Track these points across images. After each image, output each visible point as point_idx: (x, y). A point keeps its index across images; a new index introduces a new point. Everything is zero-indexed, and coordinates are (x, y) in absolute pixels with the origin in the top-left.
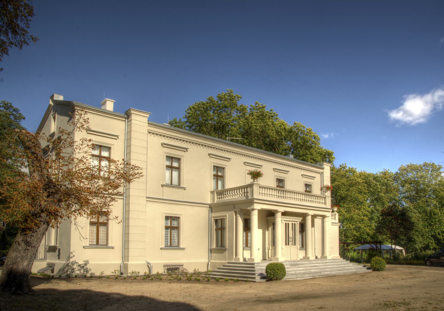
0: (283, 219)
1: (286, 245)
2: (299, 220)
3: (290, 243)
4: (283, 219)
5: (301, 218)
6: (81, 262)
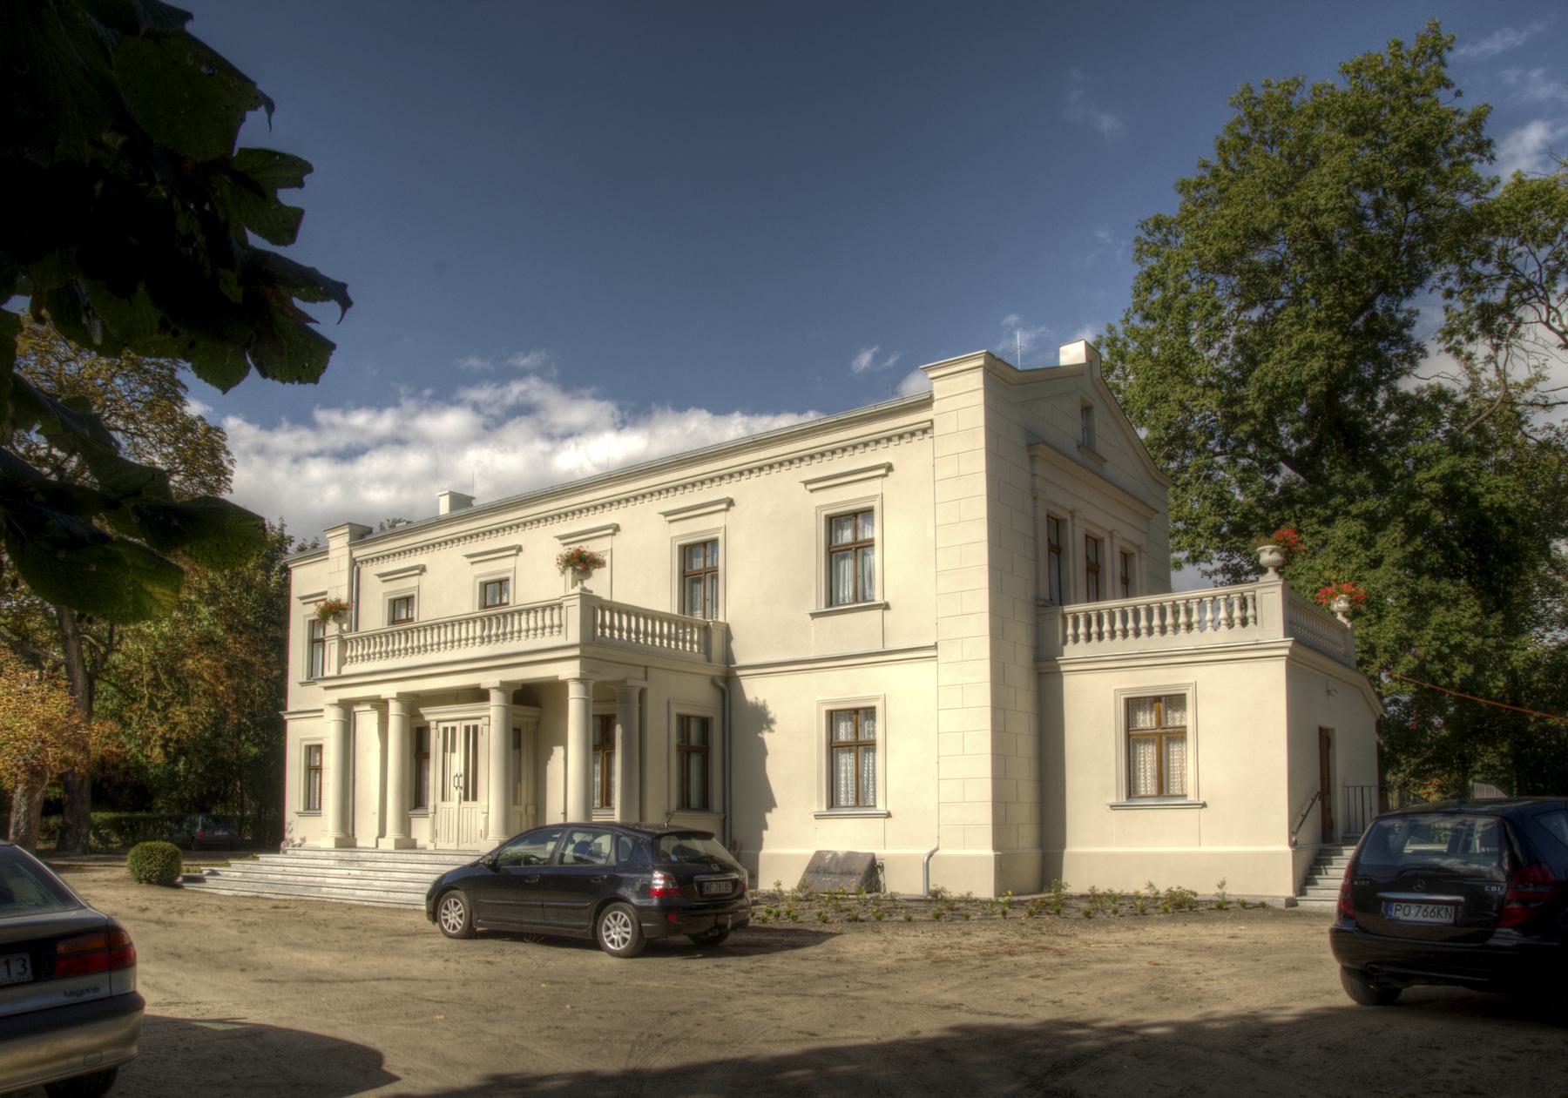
0: (355, 554)
4: (359, 553)
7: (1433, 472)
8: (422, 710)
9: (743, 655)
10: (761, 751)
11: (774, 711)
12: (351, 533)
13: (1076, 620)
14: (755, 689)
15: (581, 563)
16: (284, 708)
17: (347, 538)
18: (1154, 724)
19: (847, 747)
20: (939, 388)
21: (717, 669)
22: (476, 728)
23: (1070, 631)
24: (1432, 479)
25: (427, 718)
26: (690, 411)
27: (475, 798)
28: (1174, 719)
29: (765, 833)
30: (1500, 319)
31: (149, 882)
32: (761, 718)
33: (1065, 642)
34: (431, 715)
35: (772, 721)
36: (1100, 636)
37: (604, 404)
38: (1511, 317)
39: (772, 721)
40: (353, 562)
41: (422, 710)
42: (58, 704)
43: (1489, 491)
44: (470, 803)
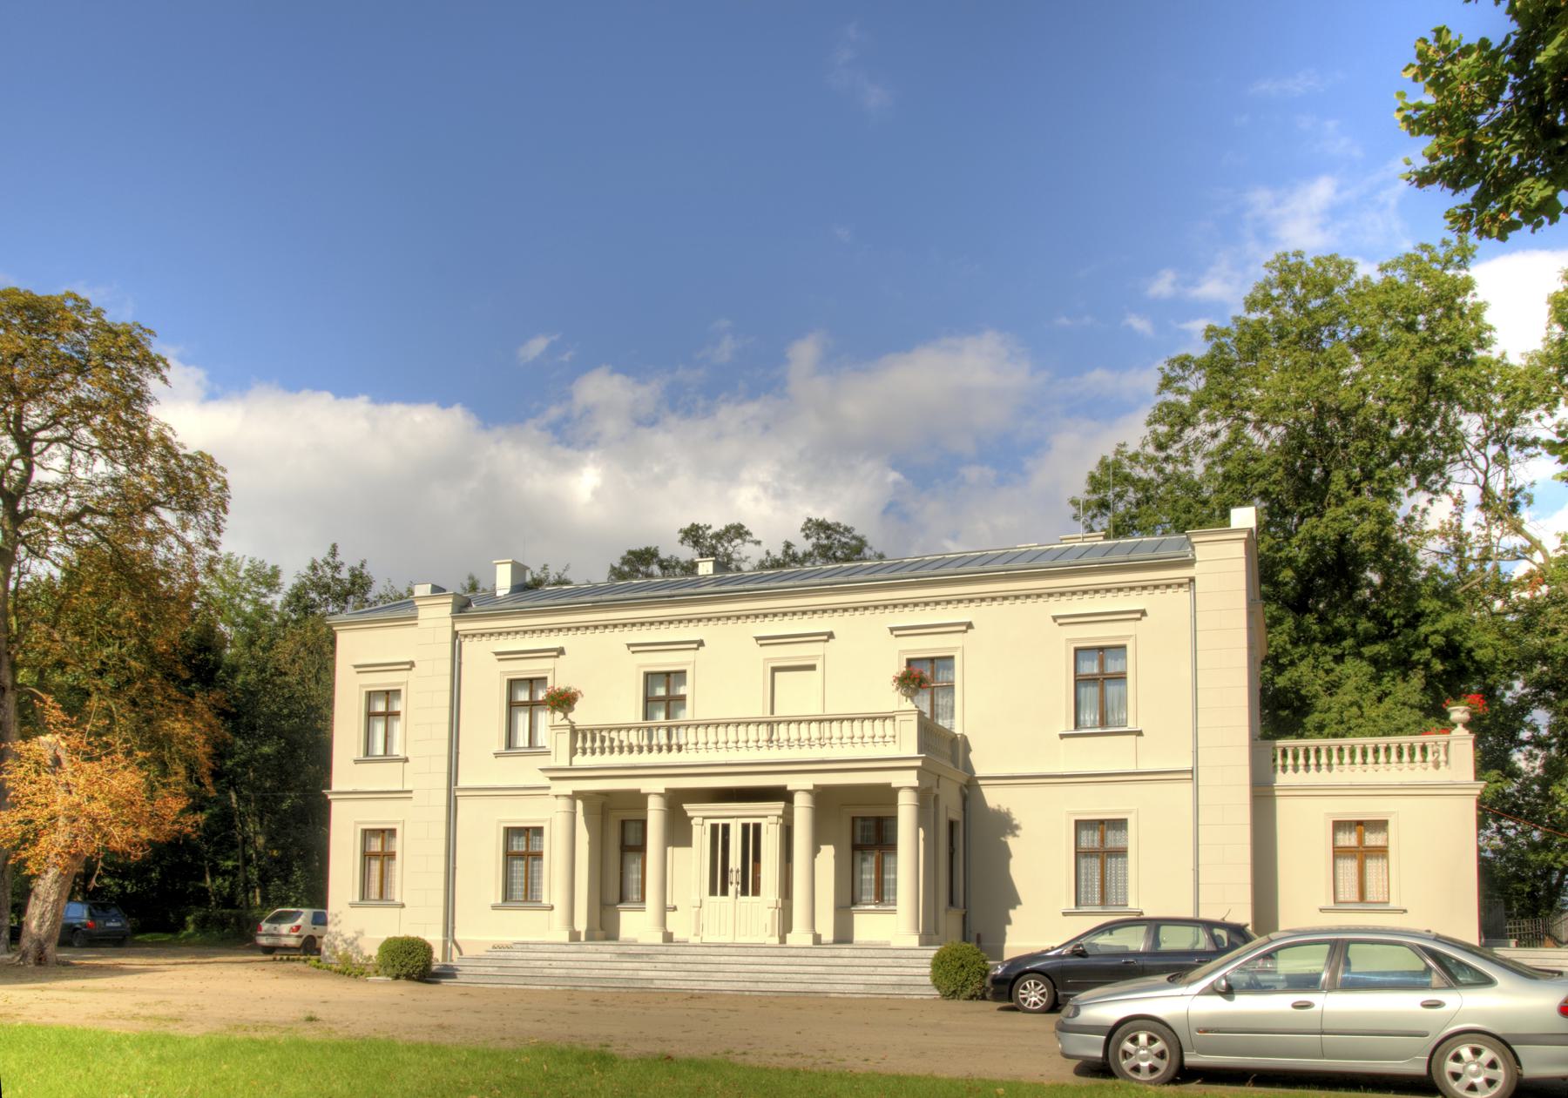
0: (457, 627)
1: (713, 892)
2: (778, 807)
3: (732, 889)
4: (461, 626)
5: (781, 804)
6: (349, 935)
7: (1438, 626)
8: (686, 806)
9: (983, 763)
10: (1006, 854)
11: (1018, 817)
12: (454, 604)
13: (1284, 754)
14: (994, 797)
15: (921, 677)
16: (329, 786)
17: (449, 609)
18: (1359, 841)
19: (520, 856)
20: (1201, 552)
21: (962, 778)
22: (757, 827)
23: (1279, 762)
24: (1436, 632)
25: (690, 814)
26: (305, 393)
27: (756, 892)
28: (1113, 839)
29: (1008, 928)
30: (1433, 477)
31: (409, 977)
32: (1004, 824)
33: (1275, 770)
34: (691, 809)
35: (1017, 827)
36: (1296, 769)
37: (192, 369)
38: (1442, 475)
39: (1017, 827)
40: (456, 634)
41: (686, 806)
42: (127, 780)
43: (1480, 646)
44: (750, 898)
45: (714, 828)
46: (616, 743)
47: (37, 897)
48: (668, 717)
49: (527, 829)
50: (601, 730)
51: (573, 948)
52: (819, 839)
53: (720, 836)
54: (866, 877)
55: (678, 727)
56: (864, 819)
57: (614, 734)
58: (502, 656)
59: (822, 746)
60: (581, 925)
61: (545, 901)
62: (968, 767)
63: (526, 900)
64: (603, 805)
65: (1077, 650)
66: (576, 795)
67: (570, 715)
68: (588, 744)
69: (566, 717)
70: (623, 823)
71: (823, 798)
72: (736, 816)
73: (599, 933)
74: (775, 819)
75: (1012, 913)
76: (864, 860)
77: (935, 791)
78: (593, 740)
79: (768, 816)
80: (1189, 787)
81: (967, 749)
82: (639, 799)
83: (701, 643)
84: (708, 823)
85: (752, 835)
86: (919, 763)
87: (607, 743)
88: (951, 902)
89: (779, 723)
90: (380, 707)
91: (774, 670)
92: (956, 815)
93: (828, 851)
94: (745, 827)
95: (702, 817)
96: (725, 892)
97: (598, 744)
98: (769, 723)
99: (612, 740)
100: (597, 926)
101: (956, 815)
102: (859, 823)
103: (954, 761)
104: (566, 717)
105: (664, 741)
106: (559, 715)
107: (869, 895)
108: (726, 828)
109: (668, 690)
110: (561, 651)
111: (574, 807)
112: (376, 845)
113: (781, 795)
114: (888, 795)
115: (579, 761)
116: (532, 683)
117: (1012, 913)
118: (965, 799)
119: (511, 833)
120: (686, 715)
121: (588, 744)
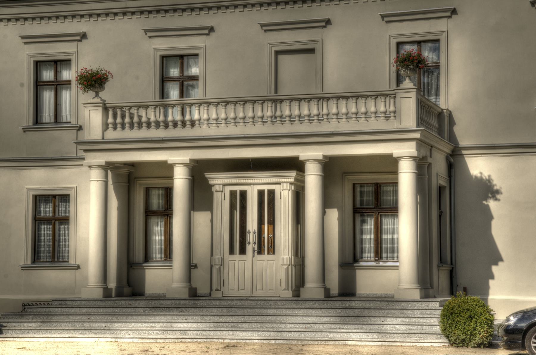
3: (249, 248)
5: (294, 173)
8: (208, 175)
22: (272, 193)
25: (211, 182)
41: (208, 175)
45: (233, 194)
46: (136, 119)
47: (249, 243)
48: (182, 94)
49: (54, 196)
50: (130, 107)
51: (108, 303)
52: (327, 202)
53: (239, 201)
54: (366, 237)
55: (192, 105)
56: (362, 185)
57: (142, 112)
58: (28, 39)
59: (301, 122)
60: (112, 284)
61: (72, 262)
62: (452, 138)
63: (53, 261)
64: (130, 175)
65: (163, 57)
66: (108, 167)
67: (101, 94)
68: (119, 120)
69: (97, 95)
70: (354, 185)
71: (331, 168)
72: (254, 184)
73: (127, 290)
74: (287, 186)
75: (494, 268)
76: (363, 222)
77: (429, 160)
78: (123, 117)
79: (283, 186)
80: (263, 92)
81: (452, 122)
82: (166, 169)
83: (84, 36)
84: (228, 189)
85: (268, 201)
86: (418, 135)
87: (127, 120)
88: (441, 260)
89: (282, 101)
90: (48, 75)
91: (277, 53)
92: (443, 182)
93: (333, 215)
94: (261, 193)
95: (221, 184)
96: (243, 251)
97: (127, 120)
98: (274, 101)
99: (131, 117)
100: (125, 282)
101: (443, 182)
102: (38, 198)
103: (440, 131)
104: (97, 95)
105: (178, 117)
106: (91, 93)
107: (369, 255)
108: (243, 194)
109: (182, 71)
110: (84, 36)
111: (106, 176)
112: (46, 210)
113: (295, 165)
114: (391, 163)
115: (111, 135)
116: (58, 64)
117: (494, 268)
118: (450, 167)
119: (39, 199)
120: (197, 94)
121: (119, 120)
